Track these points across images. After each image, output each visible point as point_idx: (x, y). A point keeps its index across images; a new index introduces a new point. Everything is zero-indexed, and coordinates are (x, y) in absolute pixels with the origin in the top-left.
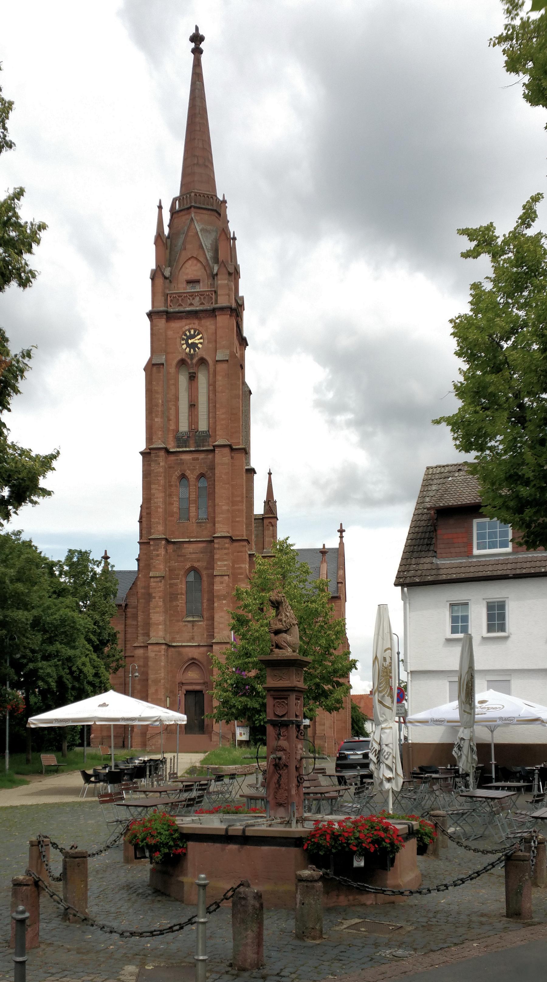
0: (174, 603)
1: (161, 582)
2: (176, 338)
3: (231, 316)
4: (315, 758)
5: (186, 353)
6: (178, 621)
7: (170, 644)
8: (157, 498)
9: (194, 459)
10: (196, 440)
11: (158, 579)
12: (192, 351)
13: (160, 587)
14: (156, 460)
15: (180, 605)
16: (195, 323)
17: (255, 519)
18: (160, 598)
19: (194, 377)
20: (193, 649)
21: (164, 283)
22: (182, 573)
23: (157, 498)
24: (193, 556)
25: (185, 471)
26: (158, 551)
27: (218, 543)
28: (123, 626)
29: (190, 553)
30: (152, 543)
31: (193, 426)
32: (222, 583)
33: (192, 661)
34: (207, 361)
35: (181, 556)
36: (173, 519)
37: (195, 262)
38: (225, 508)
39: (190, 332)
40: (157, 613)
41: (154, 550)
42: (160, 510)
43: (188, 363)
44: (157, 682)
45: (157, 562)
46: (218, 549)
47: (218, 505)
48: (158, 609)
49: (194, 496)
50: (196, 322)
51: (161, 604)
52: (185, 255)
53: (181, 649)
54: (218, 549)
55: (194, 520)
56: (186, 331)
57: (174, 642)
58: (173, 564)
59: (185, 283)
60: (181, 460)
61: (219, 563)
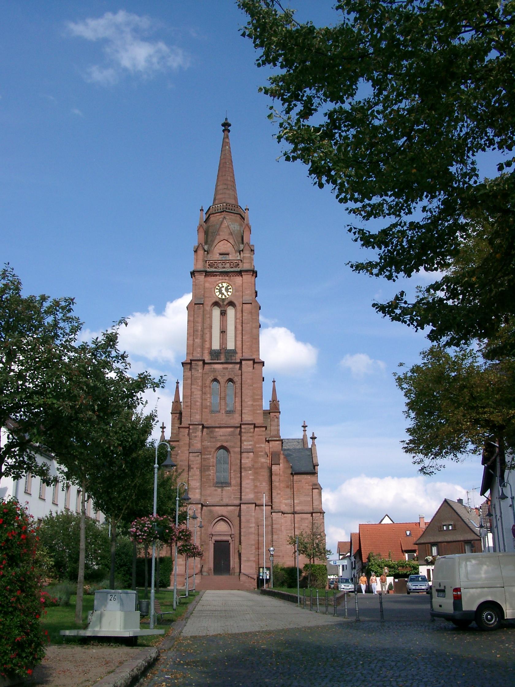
0: (207, 473)
3: (252, 275)
6: (210, 486)
8: (196, 395)
9: (224, 368)
15: (212, 474)
20: (223, 507)
21: (204, 254)
23: (196, 395)
24: (223, 438)
30: (191, 427)
32: (248, 458)
33: (221, 517)
38: (250, 403)
40: (195, 480)
42: (198, 404)
45: (195, 441)
46: (245, 432)
51: (198, 473)
52: (218, 238)
54: (245, 432)
58: (207, 444)
59: (218, 254)
60: (214, 368)
61: (245, 443)
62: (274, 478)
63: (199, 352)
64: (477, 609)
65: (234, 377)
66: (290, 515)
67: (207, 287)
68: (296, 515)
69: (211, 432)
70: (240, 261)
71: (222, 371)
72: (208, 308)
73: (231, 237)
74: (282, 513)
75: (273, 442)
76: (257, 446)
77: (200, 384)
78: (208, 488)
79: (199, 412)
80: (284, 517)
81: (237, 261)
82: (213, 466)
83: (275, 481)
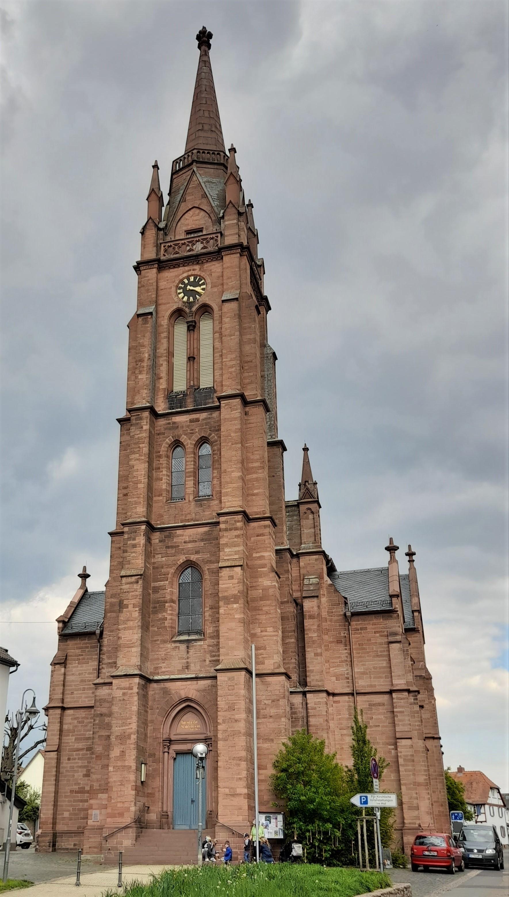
0: (160, 616)
1: (137, 582)
2: (171, 288)
4: (304, 693)
5: (184, 302)
6: (165, 642)
7: (151, 678)
9: (191, 421)
10: (195, 397)
11: (134, 579)
12: (191, 299)
13: (136, 590)
14: (137, 424)
15: (169, 617)
16: (196, 269)
17: (286, 507)
18: (134, 606)
19: (194, 327)
21: (157, 235)
22: (172, 571)
24: (190, 545)
25: (179, 436)
26: (134, 539)
27: (226, 522)
28: (96, 663)
29: (185, 542)
31: (192, 382)
32: (231, 577)
34: (212, 309)
35: (172, 547)
36: (161, 498)
37: (198, 211)
39: (188, 279)
40: (129, 628)
41: (129, 539)
42: (141, 486)
43: (185, 312)
44: (123, 738)
45: (133, 554)
46: (226, 530)
47: (225, 471)
48: (131, 623)
49: (192, 466)
50: (197, 267)
51: (136, 614)
53: (168, 685)
54: (226, 530)
55: (191, 498)
56: (184, 278)
57: (158, 674)
58: (160, 560)
60: (174, 423)
61: (227, 550)
62: (307, 623)
63: (144, 395)
64: (198, 41)
65: (210, 435)
66: (346, 698)
67: (163, 287)
68: (359, 698)
69: (169, 537)
70: (219, 235)
71: (188, 426)
72: (164, 322)
73: (204, 201)
74: (329, 694)
75: (307, 558)
76: (255, 555)
77: (146, 450)
78: (162, 646)
79: (141, 500)
80: (334, 702)
81: (214, 236)
82: (173, 601)
83: (310, 630)
